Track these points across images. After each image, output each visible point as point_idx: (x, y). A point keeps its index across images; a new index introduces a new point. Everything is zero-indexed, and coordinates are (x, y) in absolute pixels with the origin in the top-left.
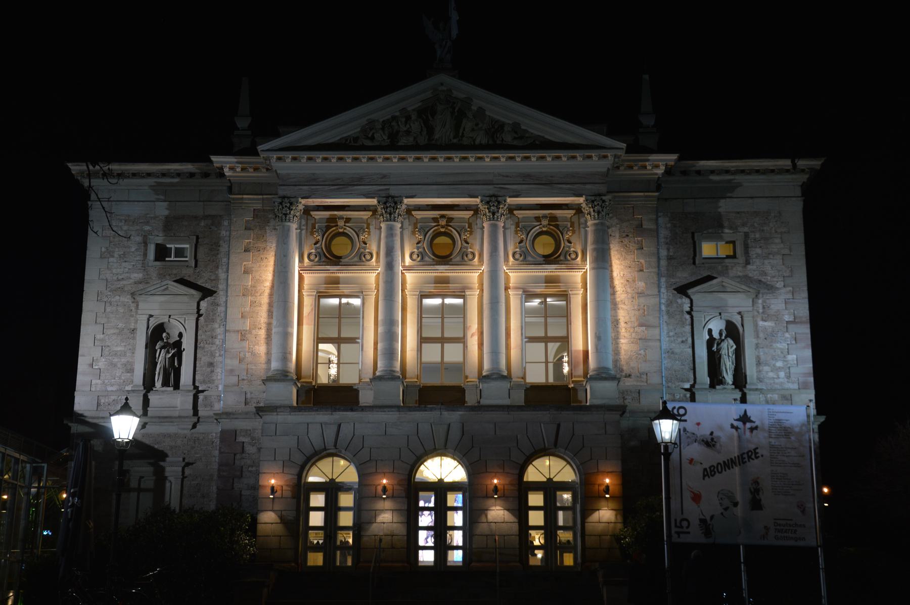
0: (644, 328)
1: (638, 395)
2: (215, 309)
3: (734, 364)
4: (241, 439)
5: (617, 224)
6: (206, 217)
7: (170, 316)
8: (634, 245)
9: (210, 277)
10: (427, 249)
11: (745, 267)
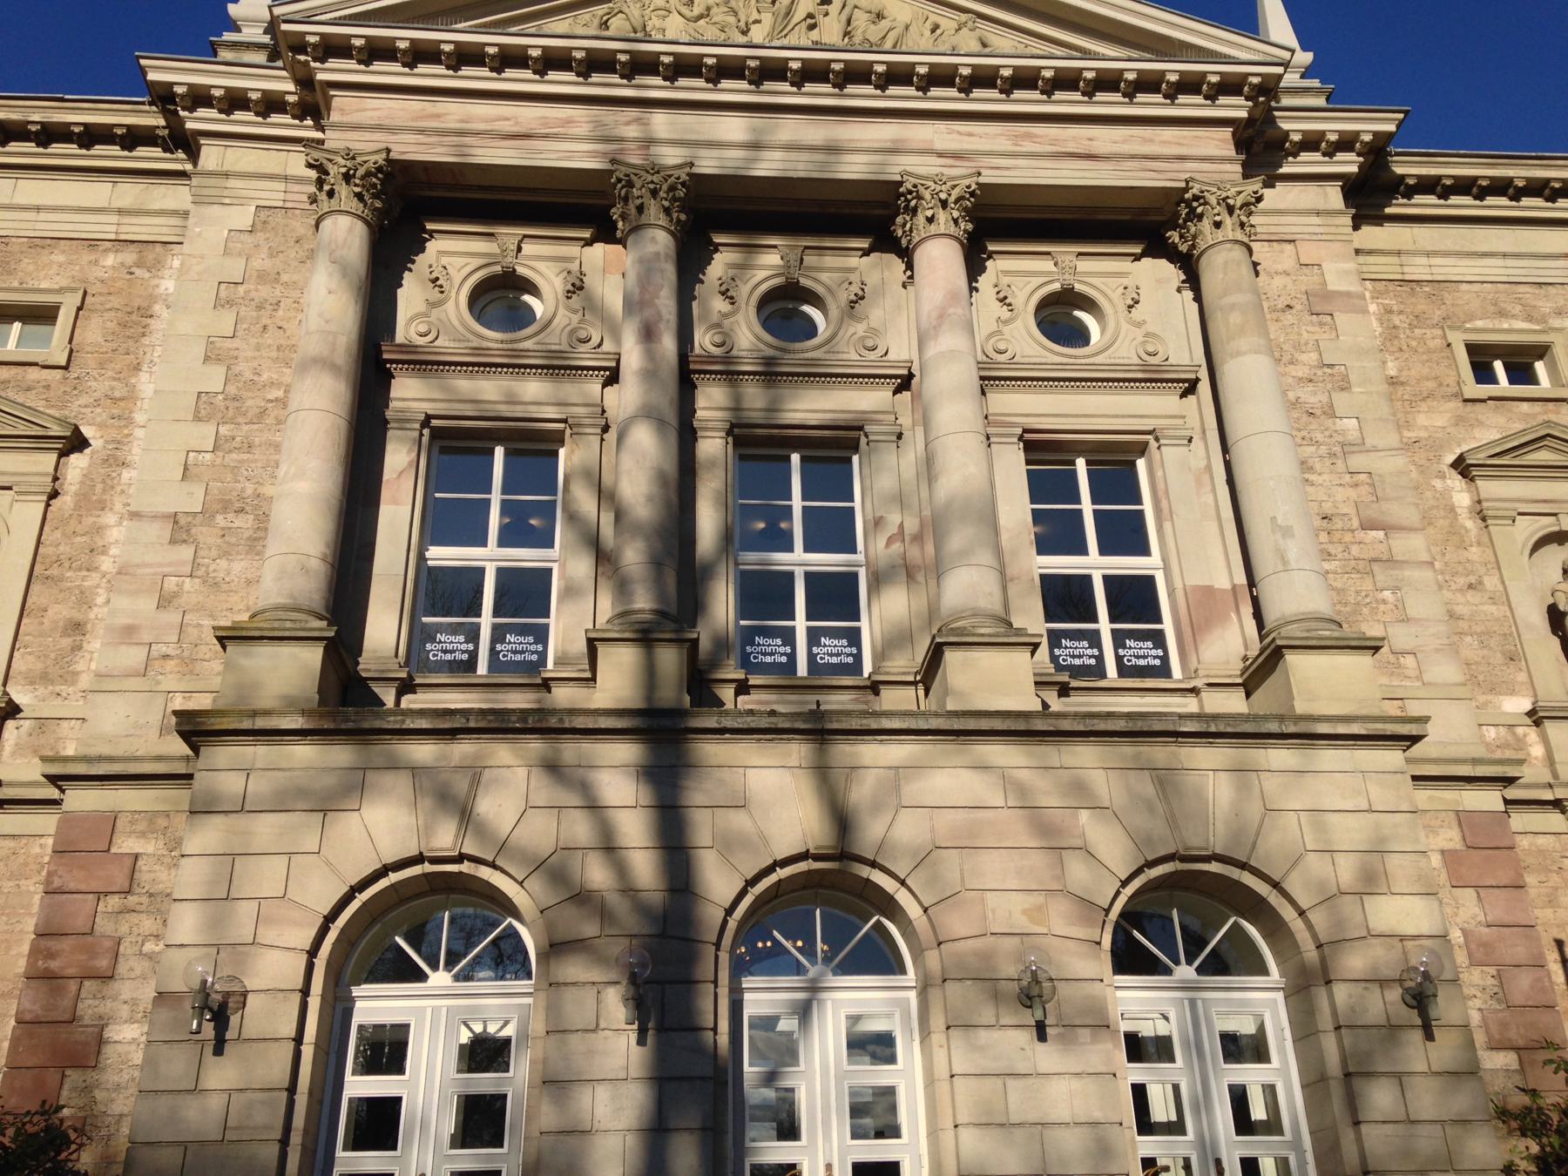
2: (114, 474)
4: (126, 844)
9: (109, 393)
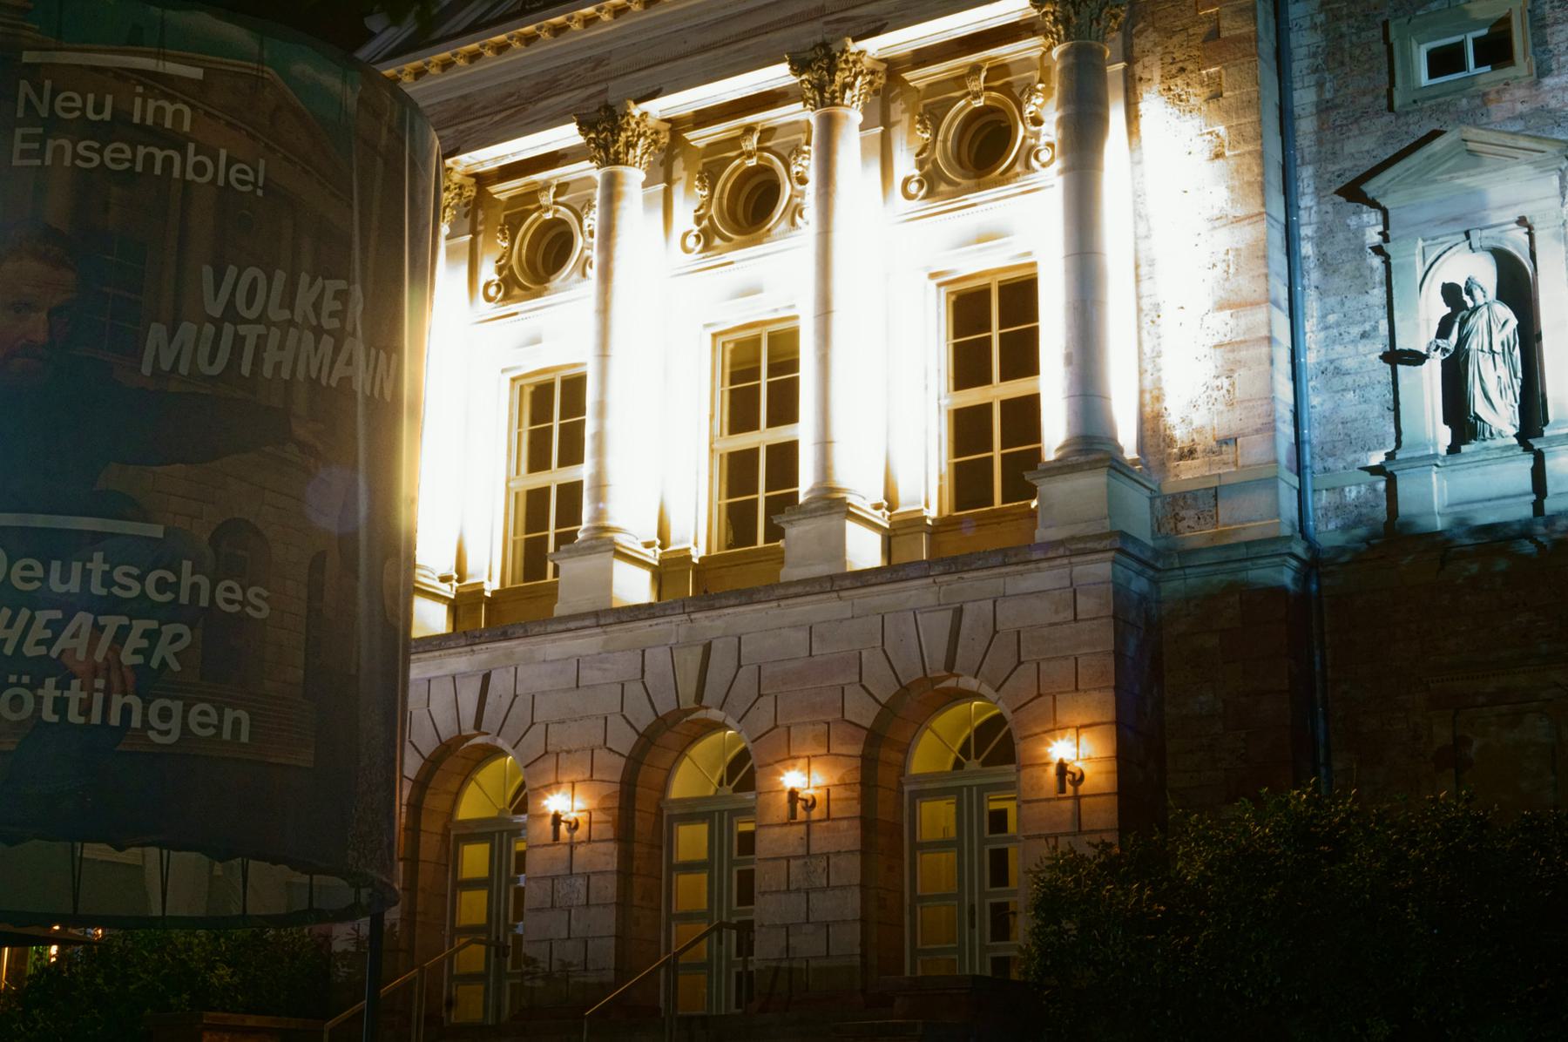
0: (1228, 312)
1: (1212, 501)
3: (1520, 375)
5: (1156, 45)
8: (1198, 90)
10: (719, 220)
11: (1536, 83)
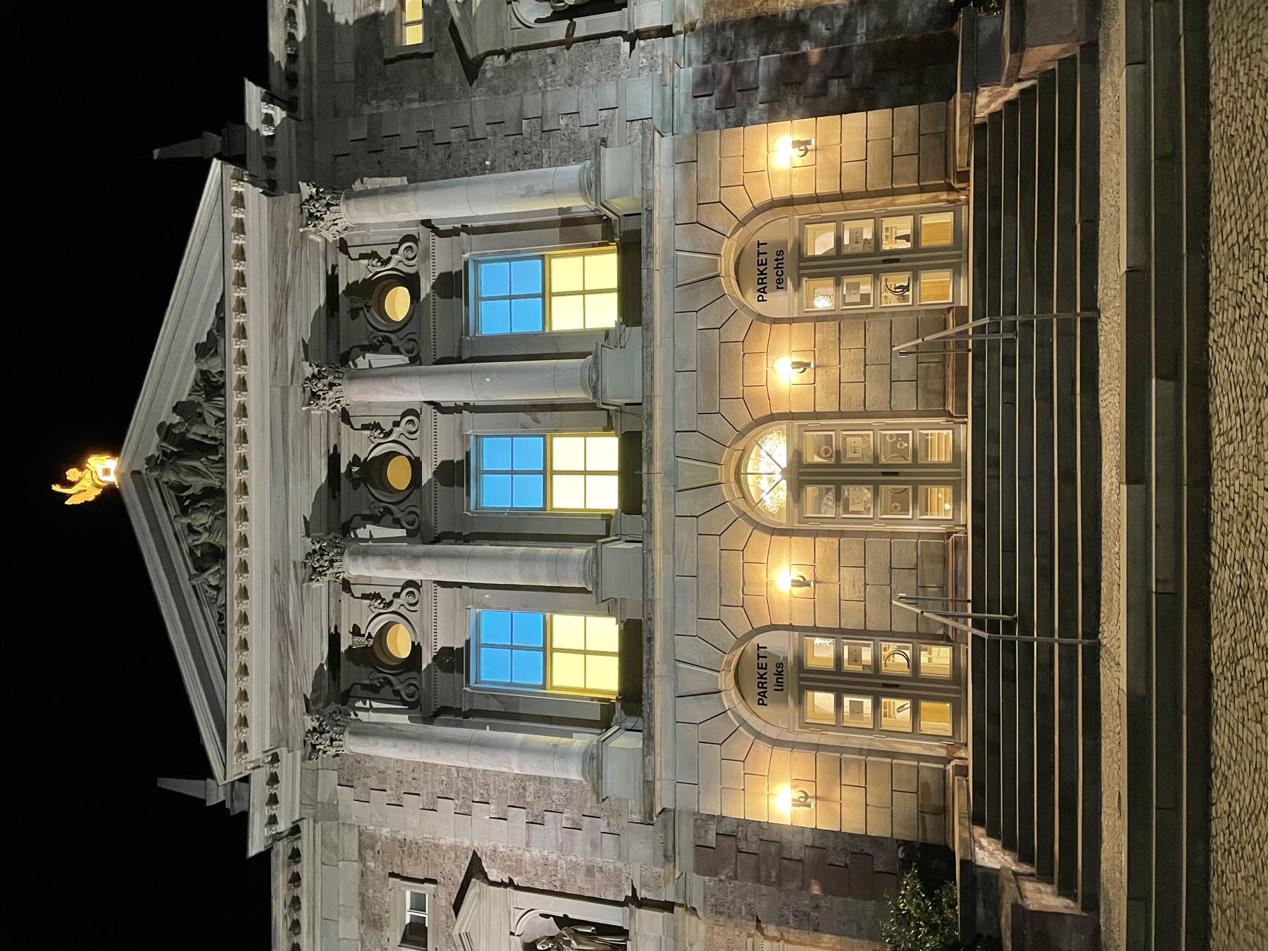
4: (711, 839)
6: (362, 858)
7: (512, 934)
